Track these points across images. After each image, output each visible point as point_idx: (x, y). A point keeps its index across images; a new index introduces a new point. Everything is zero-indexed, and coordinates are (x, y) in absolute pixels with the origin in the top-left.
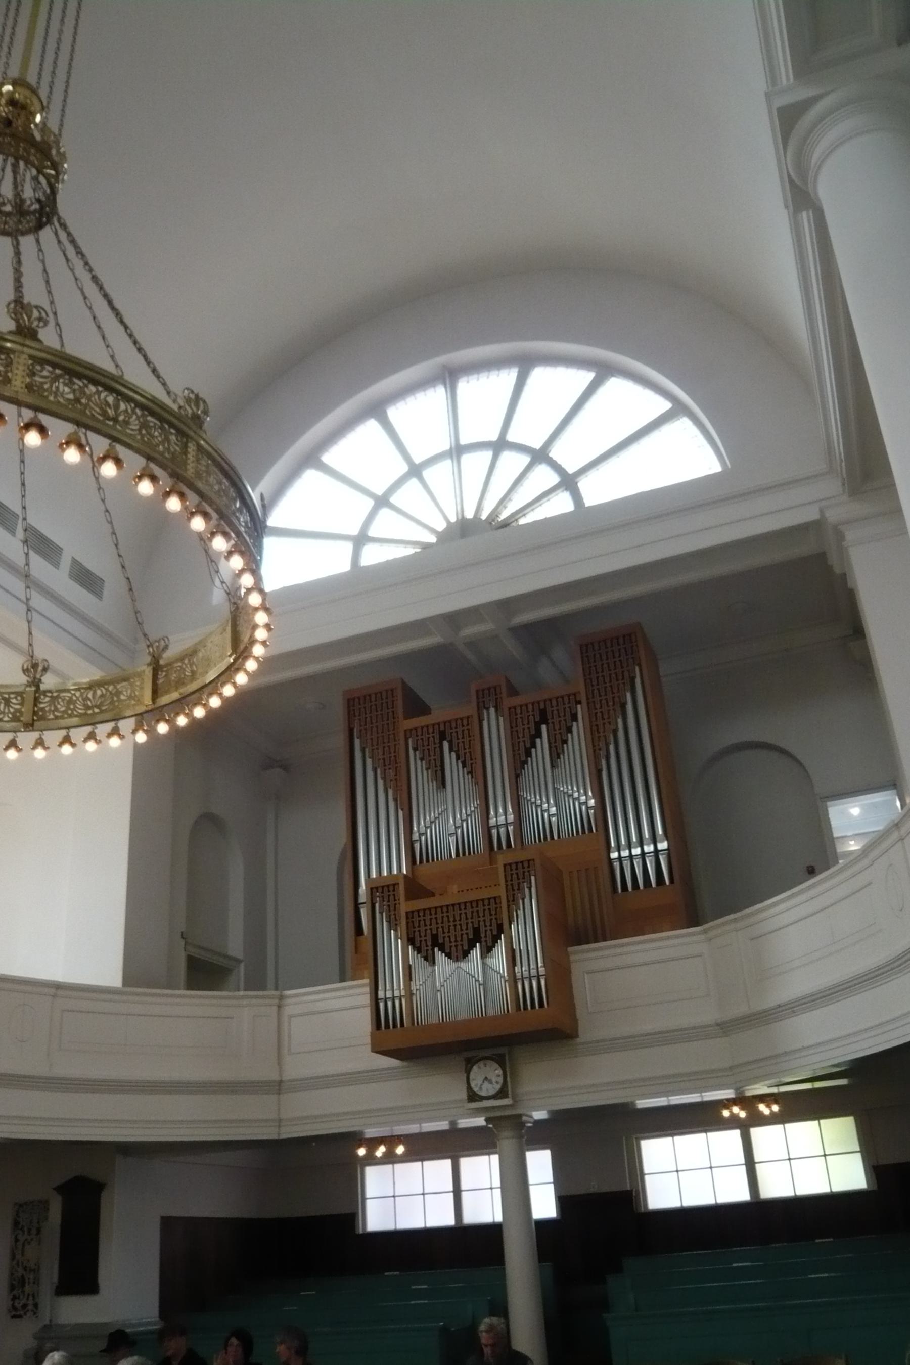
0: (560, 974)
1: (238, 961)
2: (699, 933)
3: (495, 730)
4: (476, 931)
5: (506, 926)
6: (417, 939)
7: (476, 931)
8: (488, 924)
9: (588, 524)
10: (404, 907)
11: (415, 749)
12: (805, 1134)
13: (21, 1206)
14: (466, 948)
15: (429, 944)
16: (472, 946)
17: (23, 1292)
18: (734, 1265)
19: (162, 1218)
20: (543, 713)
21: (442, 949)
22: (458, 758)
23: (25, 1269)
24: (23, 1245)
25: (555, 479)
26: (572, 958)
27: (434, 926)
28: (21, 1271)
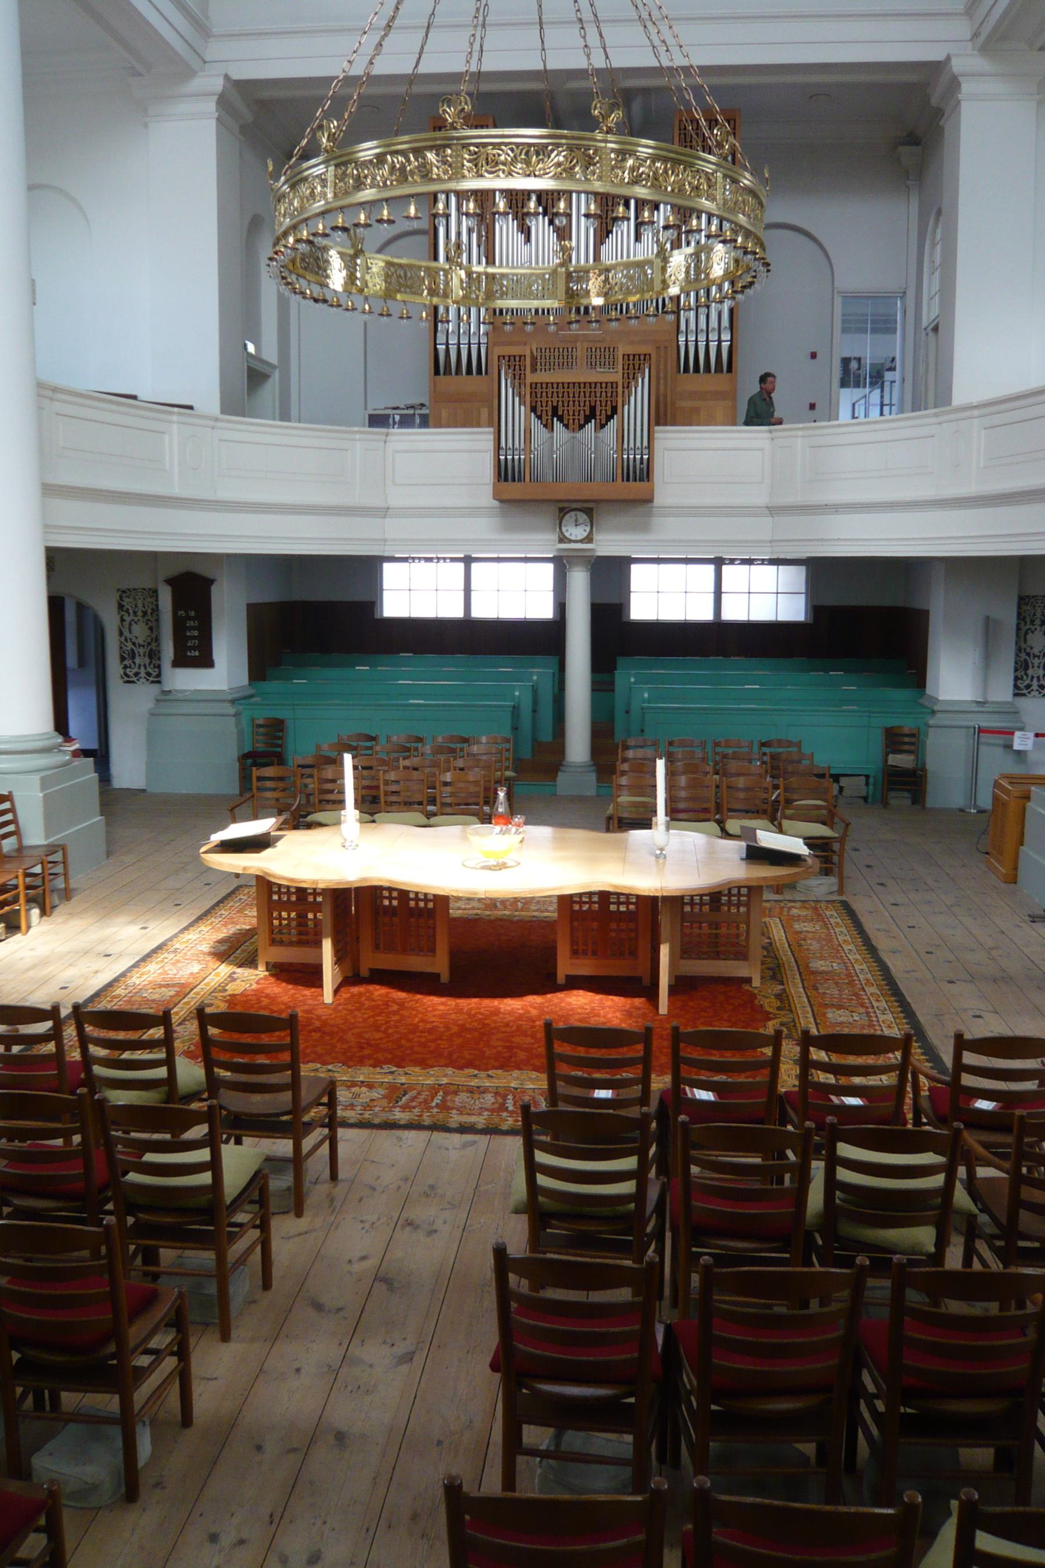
1: (273, 367)
2: (766, 431)
4: (593, 409)
5: (619, 410)
6: (539, 408)
7: (593, 409)
8: (604, 404)
10: (530, 378)
12: (766, 576)
13: (124, 592)
14: (582, 422)
15: (550, 414)
16: (587, 420)
17: (134, 663)
19: (248, 605)
21: (561, 419)
23: (134, 644)
24: (130, 624)
27: (555, 399)
28: (130, 645)
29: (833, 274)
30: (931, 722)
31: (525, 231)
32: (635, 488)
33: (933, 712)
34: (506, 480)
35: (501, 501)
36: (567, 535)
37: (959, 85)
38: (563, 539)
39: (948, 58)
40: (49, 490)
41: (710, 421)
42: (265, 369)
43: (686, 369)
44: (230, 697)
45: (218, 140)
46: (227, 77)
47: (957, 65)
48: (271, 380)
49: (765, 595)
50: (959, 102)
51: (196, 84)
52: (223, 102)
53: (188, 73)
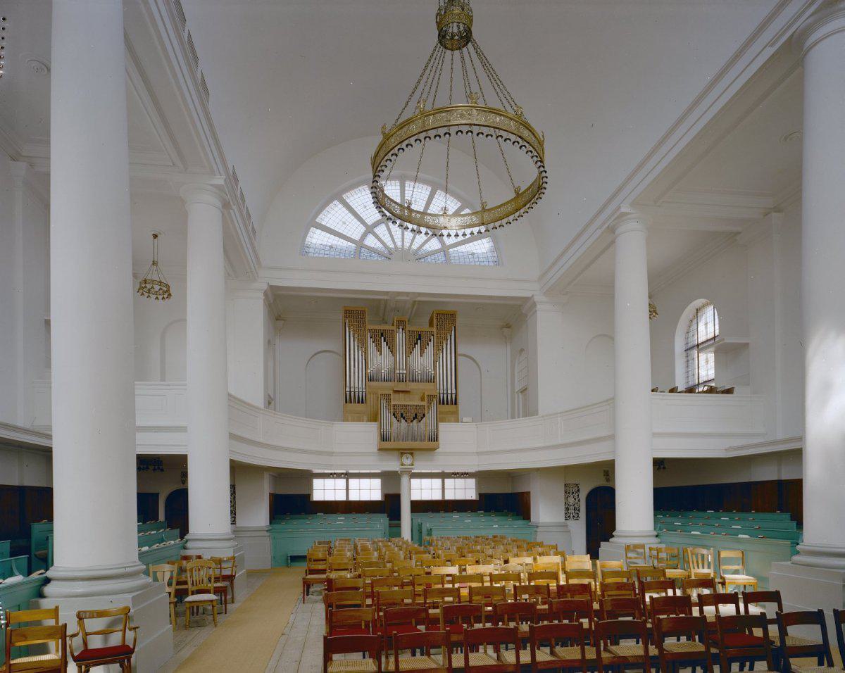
3: (400, 337)
7: (416, 414)
10: (393, 403)
11: (371, 338)
16: (414, 419)
19: (187, 455)
20: (420, 335)
21: (404, 418)
22: (387, 345)
29: (477, 364)
30: (538, 530)
32: (432, 444)
37: (536, 305)
38: (402, 465)
41: (449, 421)
44: (267, 529)
47: (536, 299)
49: (464, 490)
52: (266, 294)
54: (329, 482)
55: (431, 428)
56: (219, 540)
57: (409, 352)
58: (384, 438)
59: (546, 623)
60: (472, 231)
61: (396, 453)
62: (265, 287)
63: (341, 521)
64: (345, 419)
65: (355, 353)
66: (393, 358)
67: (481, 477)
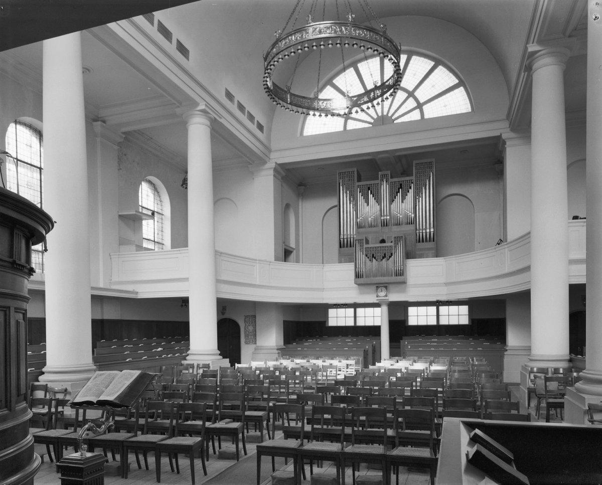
0: (404, 265)
1: (294, 249)
4: (385, 254)
7: (385, 254)
9: (425, 124)
10: (365, 246)
16: (383, 258)
18: (139, 352)
20: (401, 185)
21: (375, 258)
22: (373, 196)
25: (406, 95)
26: (408, 262)
31: (367, 202)
32: (399, 279)
33: (507, 350)
34: (358, 278)
35: (359, 285)
36: (379, 294)
38: (377, 297)
39: (501, 134)
40: (218, 281)
42: (291, 249)
43: (419, 242)
45: (274, 183)
46: (276, 163)
47: (504, 137)
48: (293, 253)
50: (506, 148)
51: (268, 166)
52: (275, 170)
53: (265, 163)
54: (341, 311)
55: (398, 266)
56: (208, 355)
57: (392, 201)
58: (358, 276)
59: (200, 423)
60: (368, 106)
61: (374, 287)
62: (273, 165)
63: (434, 342)
64: (340, 262)
65: (347, 205)
66: (378, 207)
67: (473, 304)
